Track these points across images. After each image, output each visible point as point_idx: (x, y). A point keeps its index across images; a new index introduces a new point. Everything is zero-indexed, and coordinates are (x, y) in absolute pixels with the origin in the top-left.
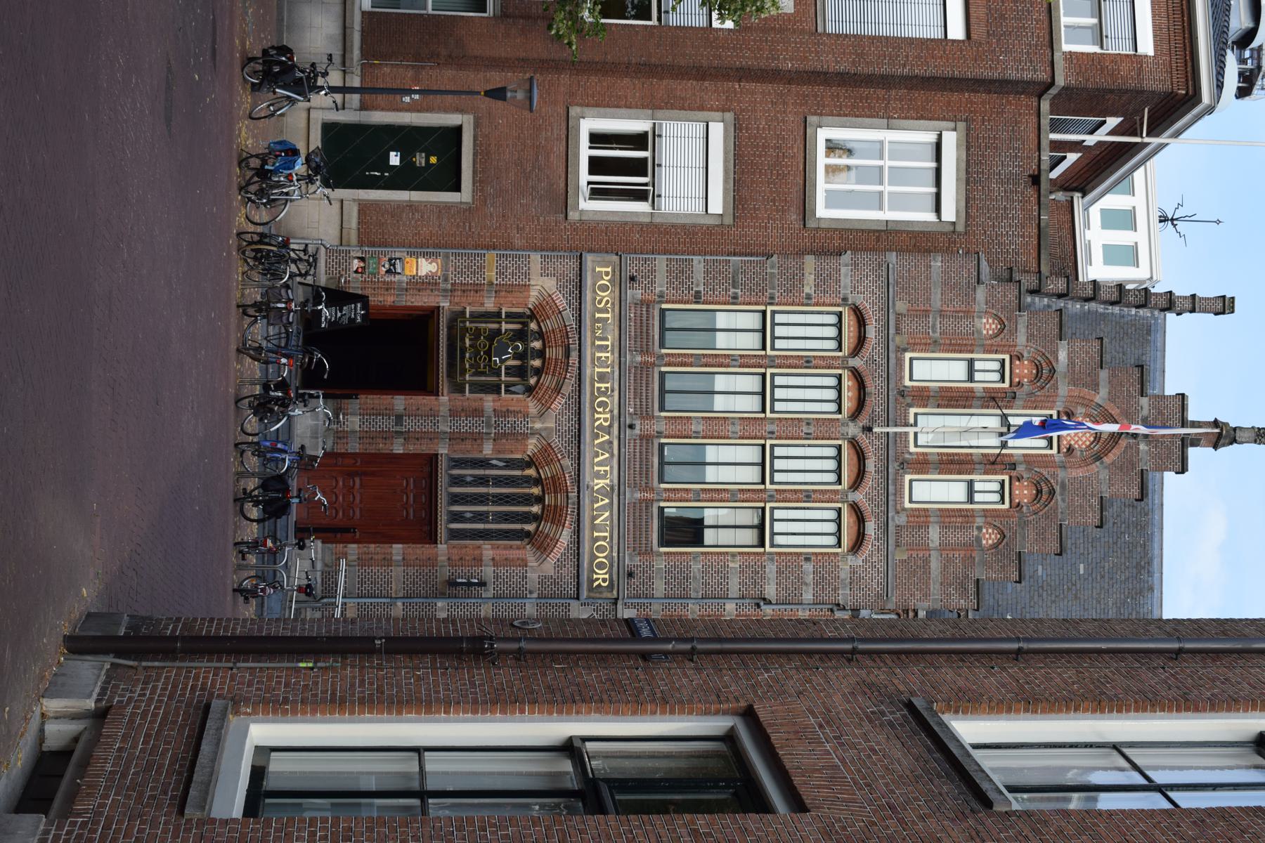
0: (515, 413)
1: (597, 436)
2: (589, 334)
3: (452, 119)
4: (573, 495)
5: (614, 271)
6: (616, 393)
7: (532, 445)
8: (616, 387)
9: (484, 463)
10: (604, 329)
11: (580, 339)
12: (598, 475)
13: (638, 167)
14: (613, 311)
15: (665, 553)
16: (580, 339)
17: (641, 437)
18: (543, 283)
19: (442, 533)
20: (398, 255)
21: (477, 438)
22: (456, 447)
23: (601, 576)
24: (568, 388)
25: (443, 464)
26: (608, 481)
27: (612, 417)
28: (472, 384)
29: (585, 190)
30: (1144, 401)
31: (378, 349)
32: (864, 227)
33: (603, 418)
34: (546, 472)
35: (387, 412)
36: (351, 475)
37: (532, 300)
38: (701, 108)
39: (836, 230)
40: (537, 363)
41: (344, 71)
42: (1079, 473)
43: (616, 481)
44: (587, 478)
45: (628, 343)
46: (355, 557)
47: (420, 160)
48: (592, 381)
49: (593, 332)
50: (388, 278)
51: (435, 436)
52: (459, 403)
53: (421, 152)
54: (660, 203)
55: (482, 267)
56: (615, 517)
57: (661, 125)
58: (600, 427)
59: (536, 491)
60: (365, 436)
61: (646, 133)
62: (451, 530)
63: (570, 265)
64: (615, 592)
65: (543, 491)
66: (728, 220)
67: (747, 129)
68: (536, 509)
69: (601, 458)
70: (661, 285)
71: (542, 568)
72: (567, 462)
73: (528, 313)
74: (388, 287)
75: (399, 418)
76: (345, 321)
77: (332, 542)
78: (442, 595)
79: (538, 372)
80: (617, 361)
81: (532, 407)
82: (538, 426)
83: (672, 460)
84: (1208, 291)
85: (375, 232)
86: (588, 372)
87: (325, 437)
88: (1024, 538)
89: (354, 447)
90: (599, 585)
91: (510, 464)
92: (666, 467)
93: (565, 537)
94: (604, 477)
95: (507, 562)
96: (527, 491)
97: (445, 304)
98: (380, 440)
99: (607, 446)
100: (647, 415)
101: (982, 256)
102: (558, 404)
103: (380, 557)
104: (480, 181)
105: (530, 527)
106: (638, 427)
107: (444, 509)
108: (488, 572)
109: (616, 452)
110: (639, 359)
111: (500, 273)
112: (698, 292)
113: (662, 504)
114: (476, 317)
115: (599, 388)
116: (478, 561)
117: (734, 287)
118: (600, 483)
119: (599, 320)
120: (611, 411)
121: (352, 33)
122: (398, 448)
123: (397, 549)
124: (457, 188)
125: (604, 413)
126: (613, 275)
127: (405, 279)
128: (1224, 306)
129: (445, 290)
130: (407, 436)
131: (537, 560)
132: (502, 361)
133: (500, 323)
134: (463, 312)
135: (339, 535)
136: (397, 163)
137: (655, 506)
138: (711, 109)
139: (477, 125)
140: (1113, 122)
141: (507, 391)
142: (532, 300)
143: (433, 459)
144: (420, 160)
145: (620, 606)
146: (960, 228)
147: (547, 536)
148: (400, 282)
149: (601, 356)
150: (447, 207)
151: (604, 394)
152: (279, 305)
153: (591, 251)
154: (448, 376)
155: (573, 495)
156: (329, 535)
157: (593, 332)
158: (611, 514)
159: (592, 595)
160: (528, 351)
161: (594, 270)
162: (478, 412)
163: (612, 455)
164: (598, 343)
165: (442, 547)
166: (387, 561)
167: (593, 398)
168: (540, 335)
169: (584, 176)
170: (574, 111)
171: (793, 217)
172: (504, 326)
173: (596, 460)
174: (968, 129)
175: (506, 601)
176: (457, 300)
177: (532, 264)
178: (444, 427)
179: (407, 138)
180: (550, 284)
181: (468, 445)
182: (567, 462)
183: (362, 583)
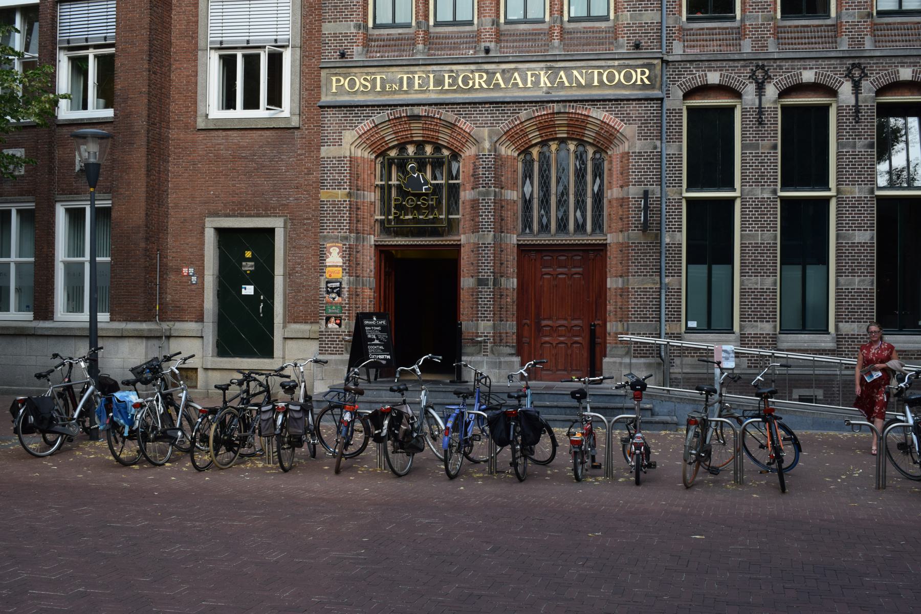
0: (475, 168)
1: (497, 85)
2: (396, 97)
3: (210, 237)
4: (556, 107)
5: (336, 74)
6: (454, 67)
7: (508, 151)
8: (448, 68)
9: (527, 204)
10: (392, 82)
11: (402, 105)
12: (536, 83)
13: (252, 62)
14: (374, 73)
16: (402, 105)
17: (498, 41)
18: (348, 144)
19: (597, 239)
20: (323, 285)
21: (500, 205)
22: (510, 226)
23: (639, 76)
24: (449, 115)
25: (528, 239)
26: (542, 73)
27: (478, 70)
28: (449, 213)
29: (275, 113)
31: (416, 305)
33: (478, 80)
34: (535, 137)
35: (475, 293)
36: (539, 329)
37: (366, 154)
40: (429, 149)
41: (168, 337)
43: (542, 65)
44: (540, 93)
45: (405, 57)
46: (620, 324)
47: (248, 267)
48: (443, 91)
49: (395, 92)
50: (345, 294)
51: (499, 248)
52: (467, 225)
53: (241, 266)
54: (283, 40)
55: (334, 203)
57: (212, 42)
58: (488, 82)
60: (499, 315)
61: (221, 57)
62: (593, 230)
63: (331, 118)
64: (655, 62)
65: (554, 139)
69: (519, 81)
70: (349, 27)
71: (631, 138)
72: (523, 115)
73: (380, 159)
74: (354, 294)
75: (481, 282)
76: (383, 336)
77: (605, 348)
78: (658, 237)
79: (438, 148)
80: (423, 68)
81: (469, 152)
82: (487, 145)
83: (522, 12)
85: (305, 310)
86: (433, 97)
87: (500, 355)
89: (510, 326)
90: (648, 78)
91: (528, 175)
92: (530, 16)
93: (598, 114)
94: (538, 77)
95: (624, 172)
97: (372, 239)
98: (503, 301)
99: (507, 75)
100: (477, 37)
102: (465, 125)
103: (619, 299)
104: (266, 209)
106: (488, 44)
107: (572, 238)
108: (634, 191)
109: (512, 66)
110: (420, 47)
111: (340, 186)
113: (566, 18)
114: (385, 210)
115: (450, 85)
116: (623, 202)
118: (544, 80)
119: (383, 87)
120: (472, 72)
121: (127, 330)
122: (513, 283)
123: (611, 283)
124: (271, 231)
125: (474, 79)
126: (339, 74)
127: (346, 278)
129: (357, 239)
130: (499, 275)
131: (622, 142)
132: (426, 183)
133: (390, 187)
134: (382, 222)
135: (598, 340)
136: (252, 287)
139: (216, 214)
141: (457, 178)
142: (366, 154)
143: (523, 249)
144: (248, 267)
145: (670, 58)
147: (598, 133)
148: (349, 283)
149: (418, 84)
150: (288, 240)
151: (455, 79)
152: (279, 421)
154: (441, 235)
155: (556, 107)
156: (598, 350)
157: (395, 92)
158: (575, 68)
159: (658, 85)
160: (415, 157)
161: (335, 94)
162: (475, 205)
163: (516, 69)
164: (405, 88)
165: (610, 238)
167: (459, 90)
168: (402, 147)
169: (262, 112)
170: (201, 124)
172: (394, 182)
173: (521, 85)
175: (664, 174)
176: (367, 228)
177: (330, 155)
178: (489, 238)
179: (229, 279)
180: (349, 136)
181: (508, 215)
182: (523, 115)
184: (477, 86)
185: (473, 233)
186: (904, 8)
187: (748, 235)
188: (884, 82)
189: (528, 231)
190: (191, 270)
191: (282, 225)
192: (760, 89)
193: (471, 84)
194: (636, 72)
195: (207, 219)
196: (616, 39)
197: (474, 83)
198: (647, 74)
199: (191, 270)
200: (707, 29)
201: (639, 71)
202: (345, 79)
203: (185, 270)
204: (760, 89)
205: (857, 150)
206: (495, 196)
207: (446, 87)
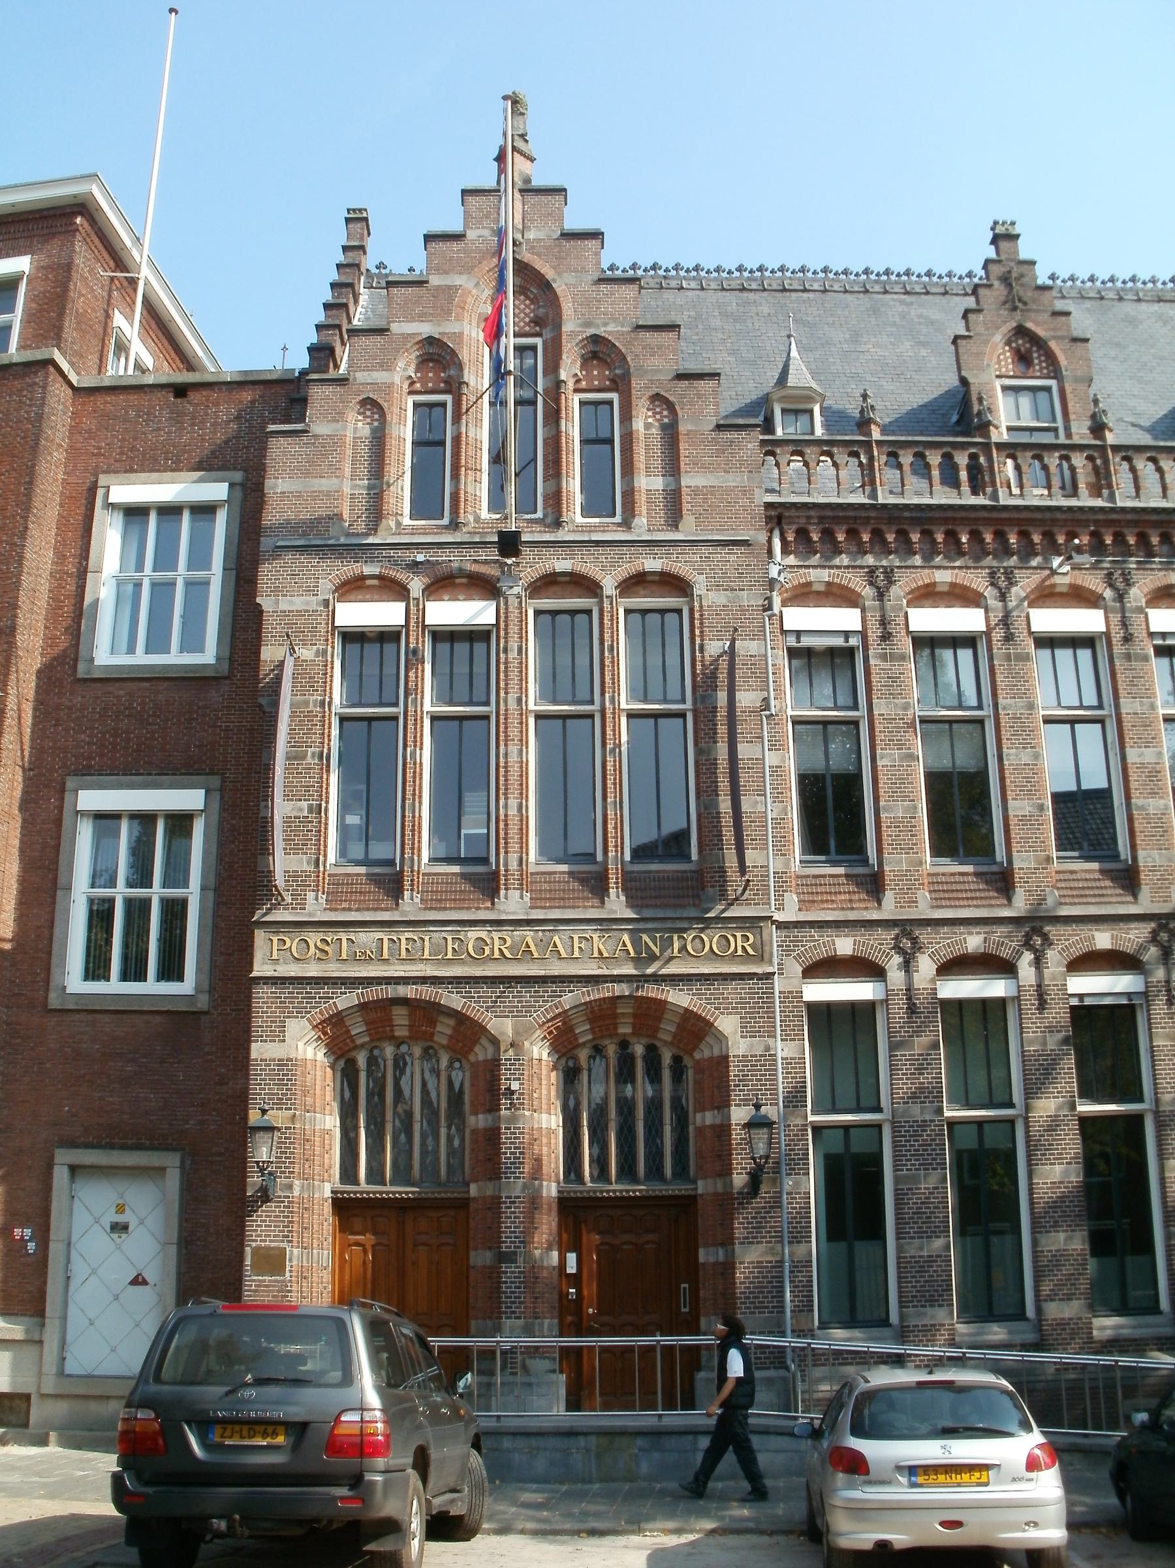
15: (700, 852)
30: (471, 235)
32: (232, 599)
38: (59, 822)
39: (233, 636)
42: (567, 308)
56: (650, 925)
65: (611, 1036)
66: (215, 781)
67: (90, 758)
68: (639, 1050)
84: (340, 236)
88: (659, 371)
101: (272, 427)
112: (310, 810)
117: (304, 757)
128: (357, 219)
137: (629, 868)
138: (61, 808)
140: (118, 320)
146: (238, 476)
169: (152, 986)
170: (54, 1001)
171: (215, 696)
174: (106, 472)
184: (497, 955)
185: (490, 1179)
186: (371, 857)
187: (906, 1176)
188: (1076, 952)
189: (572, 1176)
190: (28, 1232)
191: (178, 1164)
192: (908, 965)
193: (487, 952)
194: (735, 937)
195: (57, 1151)
196: (703, 889)
197: (492, 950)
198: (751, 941)
199: (28, 1232)
200: (831, 876)
202: (292, 941)
203: (17, 1232)
204: (908, 965)
205: (1049, 1047)
207: (450, 956)
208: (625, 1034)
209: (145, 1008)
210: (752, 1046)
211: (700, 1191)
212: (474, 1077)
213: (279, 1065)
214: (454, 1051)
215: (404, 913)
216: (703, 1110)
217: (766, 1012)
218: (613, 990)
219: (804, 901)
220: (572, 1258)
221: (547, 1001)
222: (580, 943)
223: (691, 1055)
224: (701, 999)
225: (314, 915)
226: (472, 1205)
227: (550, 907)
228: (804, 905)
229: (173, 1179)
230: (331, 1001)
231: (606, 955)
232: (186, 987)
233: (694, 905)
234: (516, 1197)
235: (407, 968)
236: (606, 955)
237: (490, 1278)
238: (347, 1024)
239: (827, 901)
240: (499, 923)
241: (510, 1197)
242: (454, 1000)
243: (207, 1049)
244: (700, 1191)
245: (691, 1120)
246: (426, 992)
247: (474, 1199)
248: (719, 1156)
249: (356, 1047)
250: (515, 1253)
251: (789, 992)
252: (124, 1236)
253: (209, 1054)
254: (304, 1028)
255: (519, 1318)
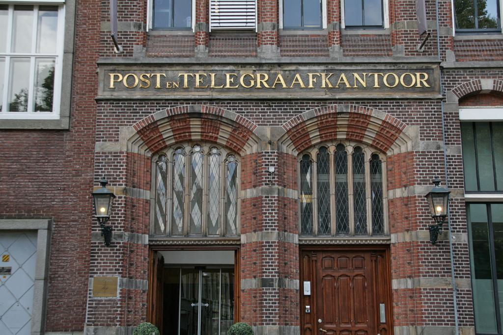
4: (340, 108)
5: (113, 71)
7: (289, 149)
12: (317, 84)
19: (377, 240)
22: (292, 225)
25: (308, 239)
26: (323, 75)
43: (323, 68)
51: (283, 247)
59: (332, 149)
64: (434, 66)
65: (332, 141)
68: (350, 149)
69: (300, 81)
72: (306, 114)
75: (265, 283)
94: (320, 77)
96: (332, 158)
105: (368, 154)
109: (293, 68)
115: (231, 84)
119: (163, 85)
126: (119, 71)
129: (131, 238)
151: (236, 78)
153: (94, 91)
155: (340, 108)
157: (175, 89)
158: (356, 71)
161: (113, 90)
166: (413, 294)
167: (241, 89)
178: (274, 237)
183: (440, 321)
184: (259, 86)
193: (253, 83)
194: (415, 75)
197: (256, 82)
200: (476, 41)
201: (418, 74)
202: (123, 77)
206: (278, 194)
207: (228, 86)
208: (341, 140)
209: (26, 128)
210: (428, 145)
211: (393, 241)
212: (244, 165)
213: (114, 156)
214: (230, 149)
215: (197, 58)
216: (394, 188)
217: (437, 124)
218: (336, 108)
219: (459, 56)
220: (307, 285)
221: (293, 115)
222: (313, 78)
223: (385, 153)
224: (393, 115)
225: (138, 60)
226: (242, 249)
227: (294, 56)
228: (458, 58)
229: (42, 238)
230: (150, 115)
231: (330, 86)
232: (55, 115)
233: (388, 55)
234: (272, 242)
235: (201, 93)
236: (330, 86)
237: (255, 297)
238: (161, 130)
239: (475, 55)
240: (260, 65)
241: (269, 242)
242: (232, 114)
243: (67, 153)
244: (393, 241)
245: (384, 195)
246: (214, 109)
247: (244, 245)
248: (407, 218)
249: (166, 147)
250: (272, 280)
251: (450, 113)
252: (8, 276)
253: (68, 157)
254: (132, 132)
255: (275, 324)
